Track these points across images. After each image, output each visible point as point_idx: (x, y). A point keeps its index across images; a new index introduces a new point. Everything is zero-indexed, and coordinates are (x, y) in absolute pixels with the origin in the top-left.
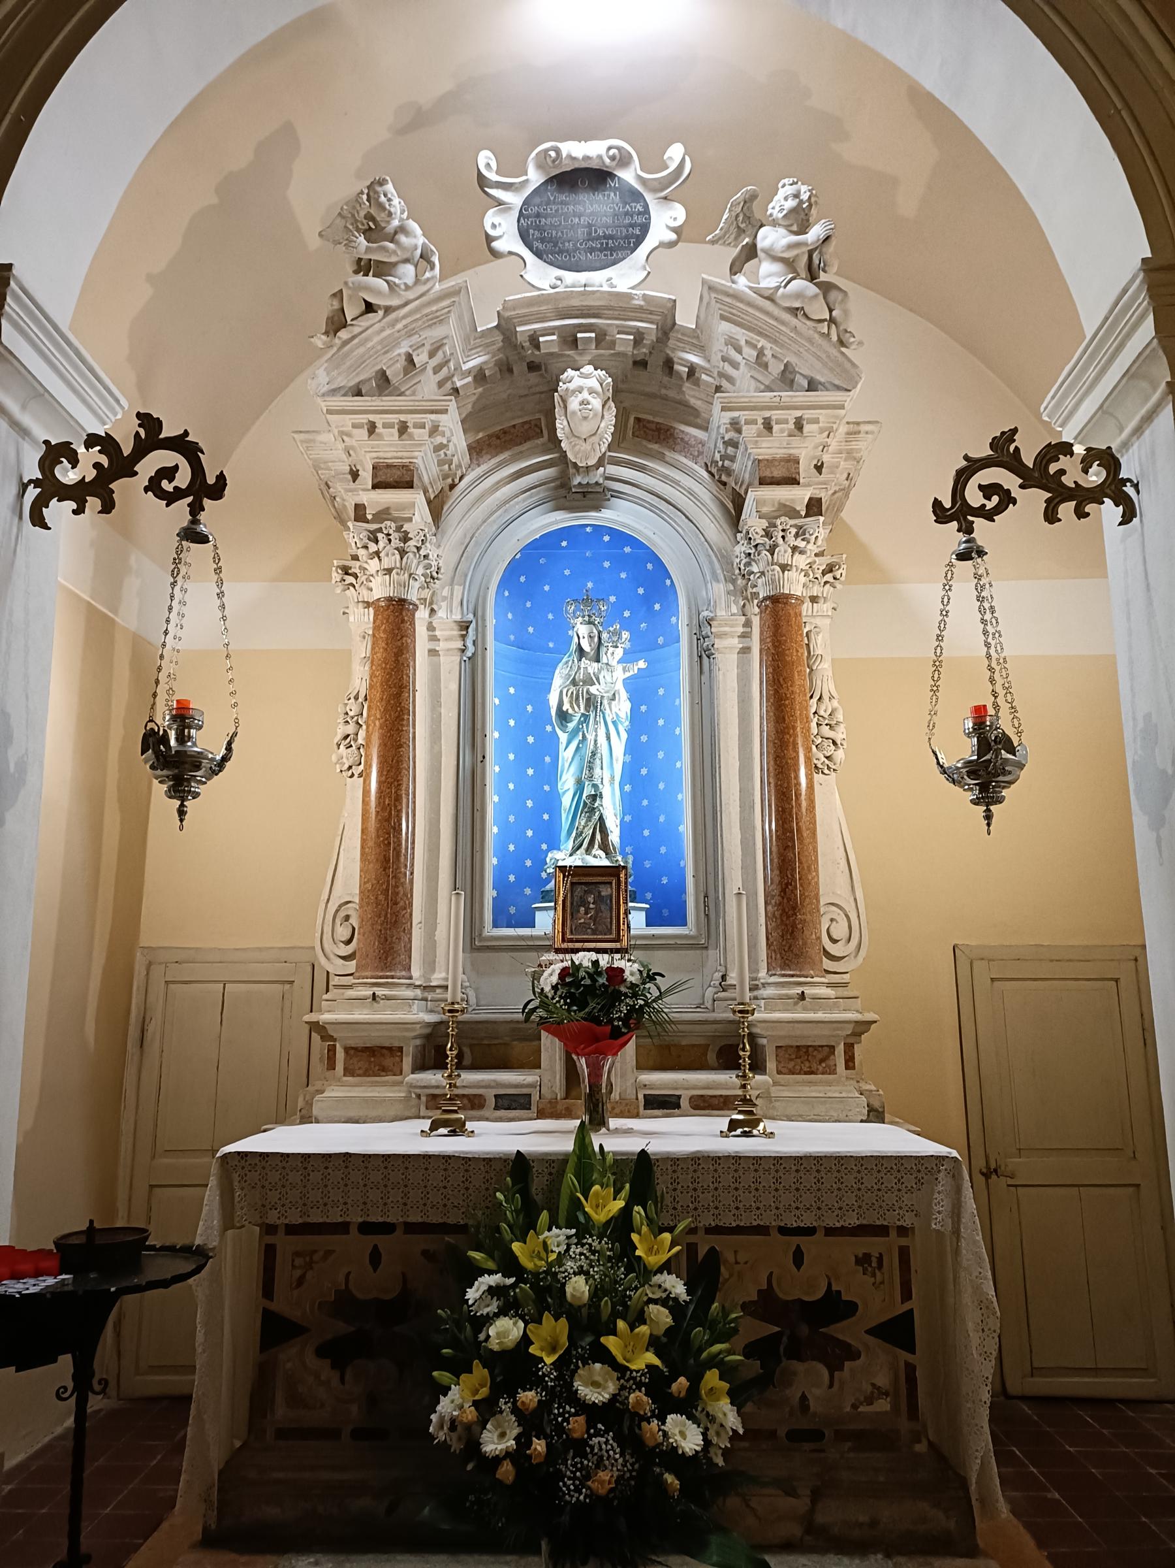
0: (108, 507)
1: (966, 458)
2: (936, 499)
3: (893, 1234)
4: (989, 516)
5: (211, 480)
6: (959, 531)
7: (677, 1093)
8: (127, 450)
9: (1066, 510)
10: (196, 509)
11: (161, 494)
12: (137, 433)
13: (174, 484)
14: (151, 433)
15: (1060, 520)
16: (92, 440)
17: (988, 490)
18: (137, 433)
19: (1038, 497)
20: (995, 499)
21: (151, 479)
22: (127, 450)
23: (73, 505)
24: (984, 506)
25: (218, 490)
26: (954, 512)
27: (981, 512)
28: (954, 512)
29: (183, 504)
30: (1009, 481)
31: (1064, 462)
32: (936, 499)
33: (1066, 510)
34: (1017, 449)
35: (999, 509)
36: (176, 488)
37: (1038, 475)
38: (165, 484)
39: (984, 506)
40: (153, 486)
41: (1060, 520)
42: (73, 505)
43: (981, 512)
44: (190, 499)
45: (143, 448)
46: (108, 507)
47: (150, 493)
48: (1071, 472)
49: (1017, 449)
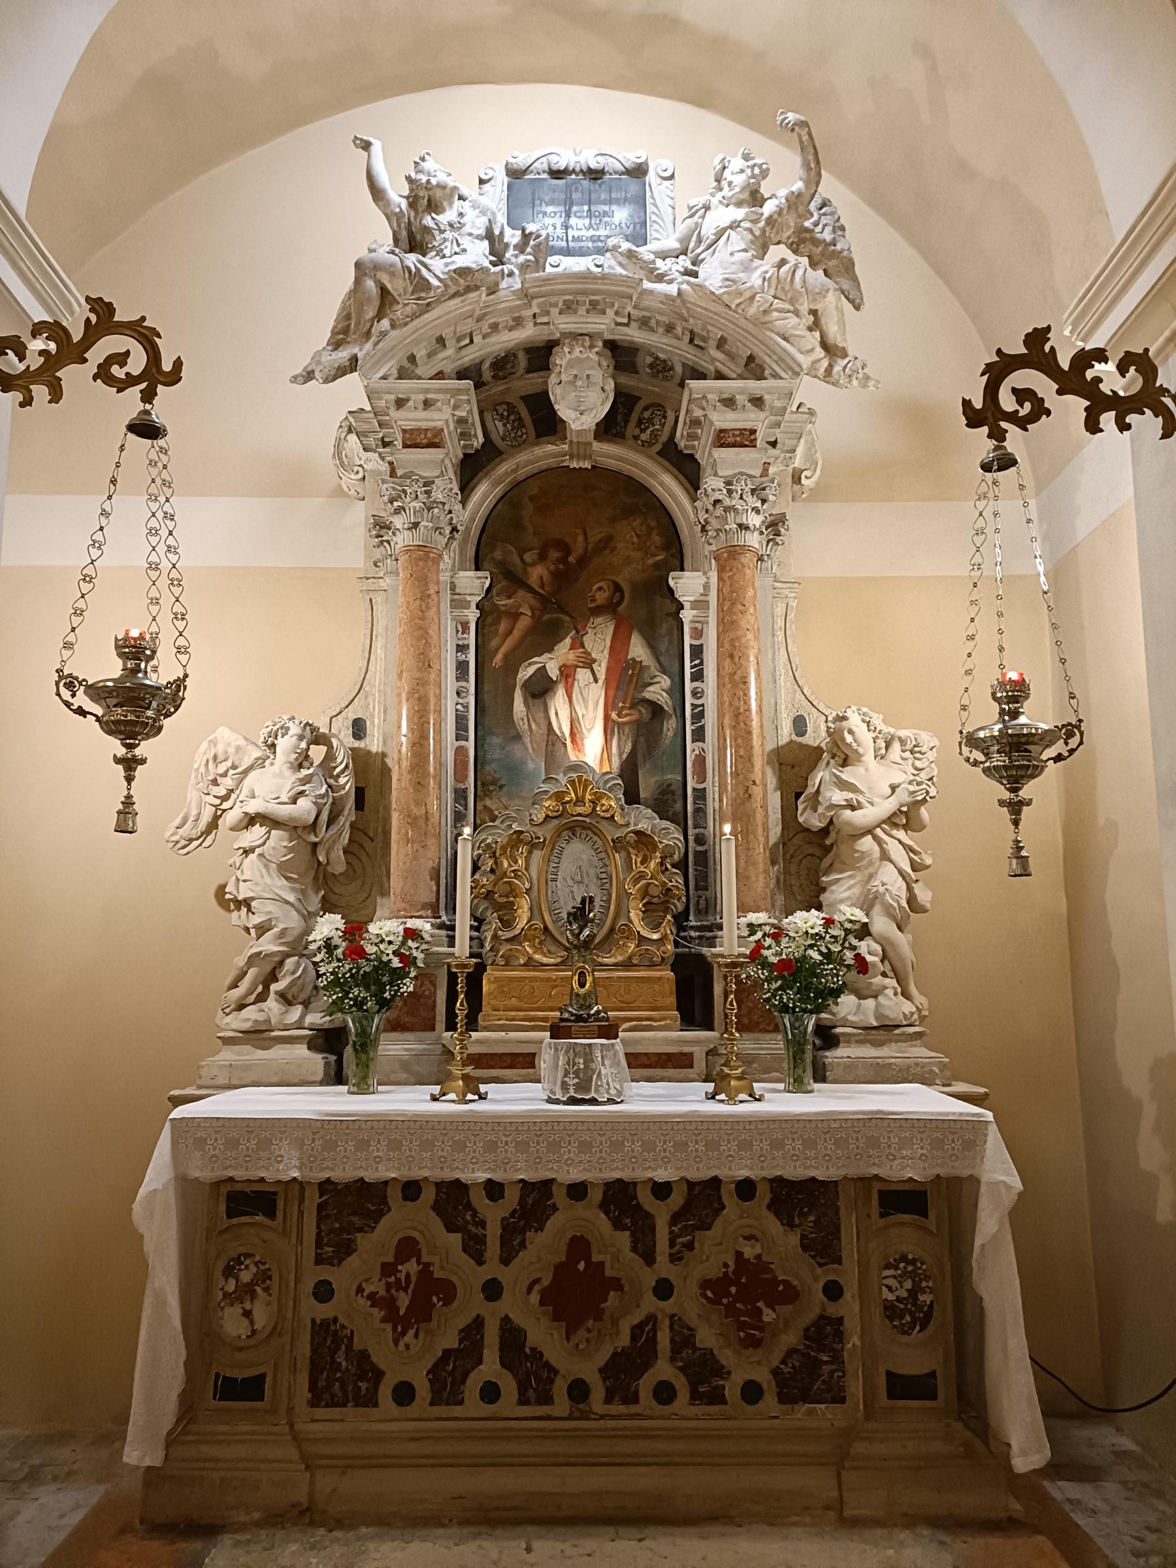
0: (56, 395)
1: (999, 352)
2: (964, 400)
3: (825, 1275)
4: (1023, 423)
5: (167, 366)
6: (989, 437)
7: (687, 1049)
8: (77, 335)
9: (1108, 419)
10: (148, 396)
11: (110, 380)
12: (88, 321)
13: (126, 369)
14: (103, 317)
15: (1102, 431)
16: (37, 330)
17: (1022, 395)
18: (88, 321)
19: (1077, 405)
20: (1028, 406)
21: (99, 366)
22: (77, 335)
23: (19, 396)
24: (1017, 411)
25: (174, 377)
26: (983, 416)
27: (1012, 417)
28: (983, 416)
29: (135, 391)
30: (1044, 386)
31: (1099, 368)
32: (964, 400)
33: (1108, 419)
34: (1052, 348)
35: (1033, 417)
36: (127, 374)
37: (1075, 380)
38: (116, 370)
39: (1017, 411)
40: (103, 374)
41: (1102, 431)
42: (19, 396)
43: (1012, 417)
44: (144, 385)
45: (93, 333)
46: (56, 395)
47: (99, 381)
48: (1109, 376)
49: (1052, 348)
